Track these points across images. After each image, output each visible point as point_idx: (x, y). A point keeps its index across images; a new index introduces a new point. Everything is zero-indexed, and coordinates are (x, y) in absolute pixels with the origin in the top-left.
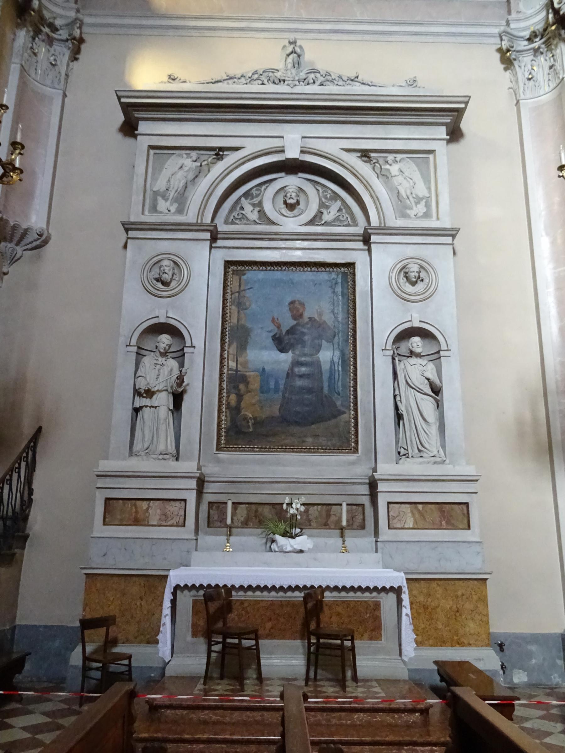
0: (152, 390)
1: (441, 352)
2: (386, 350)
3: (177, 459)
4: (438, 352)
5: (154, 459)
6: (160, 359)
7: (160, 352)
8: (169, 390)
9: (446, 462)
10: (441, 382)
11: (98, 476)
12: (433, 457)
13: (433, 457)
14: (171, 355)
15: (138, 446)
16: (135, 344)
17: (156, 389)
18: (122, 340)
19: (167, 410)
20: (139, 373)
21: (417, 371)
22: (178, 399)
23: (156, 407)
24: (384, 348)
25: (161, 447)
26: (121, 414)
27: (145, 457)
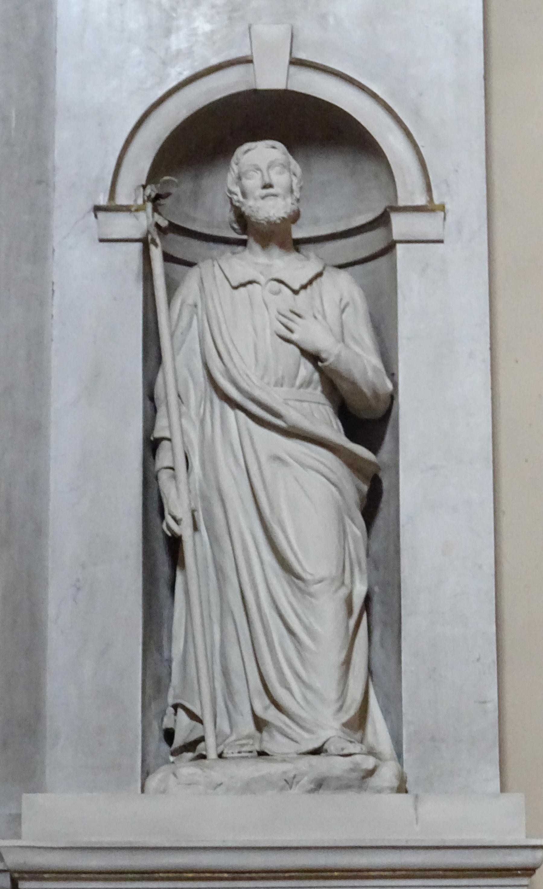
1: (396, 219)
2: (111, 208)
4: (382, 221)
9: (374, 781)
10: (392, 375)
12: (317, 752)
13: (317, 752)
21: (257, 315)
24: (103, 200)
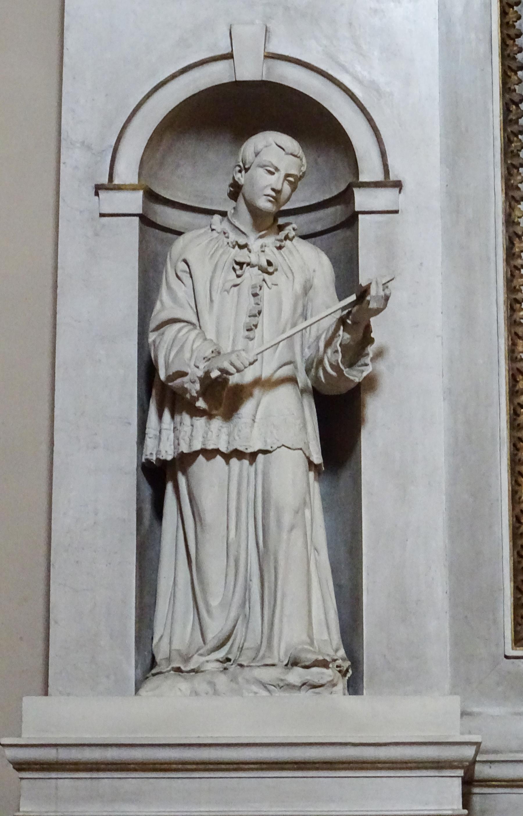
0: (234, 379)
3: (354, 687)
5: (265, 686)
6: (255, 242)
7: (255, 213)
8: (303, 378)
11: (21, 766)
14: (295, 224)
15: (175, 630)
16: (134, 180)
17: (249, 376)
18: (79, 166)
19: (304, 464)
20: (165, 307)
22: (340, 416)
23: (253, 457)
25: (291, 635)
26: (97, 490)
27: (222, 680)
